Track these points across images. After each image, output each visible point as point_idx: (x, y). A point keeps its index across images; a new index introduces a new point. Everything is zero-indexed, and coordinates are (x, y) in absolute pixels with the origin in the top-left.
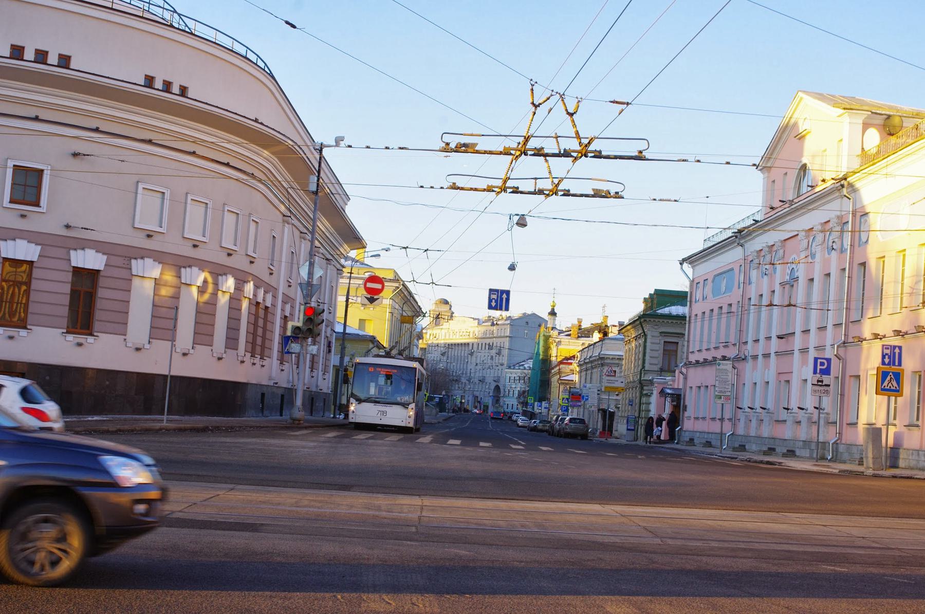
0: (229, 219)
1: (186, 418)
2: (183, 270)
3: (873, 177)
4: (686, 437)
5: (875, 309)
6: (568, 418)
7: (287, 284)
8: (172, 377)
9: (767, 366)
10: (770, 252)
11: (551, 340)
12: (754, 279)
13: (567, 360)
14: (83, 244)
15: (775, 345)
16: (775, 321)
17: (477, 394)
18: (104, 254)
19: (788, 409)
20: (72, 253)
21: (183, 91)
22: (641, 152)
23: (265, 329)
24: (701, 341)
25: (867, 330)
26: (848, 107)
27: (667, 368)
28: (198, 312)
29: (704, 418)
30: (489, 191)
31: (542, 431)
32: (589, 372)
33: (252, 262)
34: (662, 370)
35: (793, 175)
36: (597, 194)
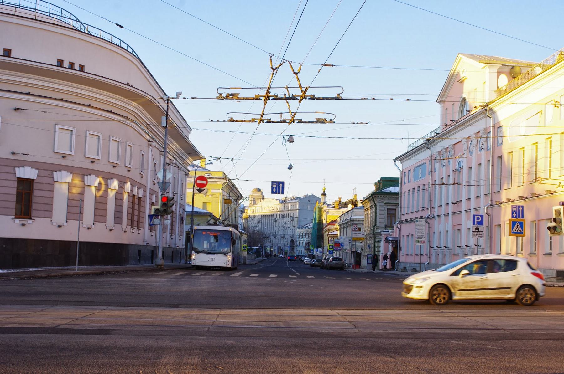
0: (114, 145)
1: (91, 267)
2: (86, 177)
3: (502, 105)
4: (401, 266)
5: (508, 184)
6: (331, 258)
7: (153, 183)
8: (80, 242)
9: (447, 221)
10: (446, 152)
11: (323, 211)
12: (437, 169)
13: (333, 222)
14: (23, 164)
15: (451, 208)
16: (450, 194)
17: (280, 245)
18: (36, 169)
19: (460, 247)
20: (17, 169)
21: (82, 68)
22: (338, 95)
23: (139, 211)
24: (408, 208)
25: (504, 197)
26: (488, 62)
27: (389, 225)
28: (96, 202)
29: (411, 254)
30: (253, 122)
31: (317, 266)
32: (345, 229)
33: (129, 171)
34: (386, 226)
35: (458, 105)
36: (319, 121)
